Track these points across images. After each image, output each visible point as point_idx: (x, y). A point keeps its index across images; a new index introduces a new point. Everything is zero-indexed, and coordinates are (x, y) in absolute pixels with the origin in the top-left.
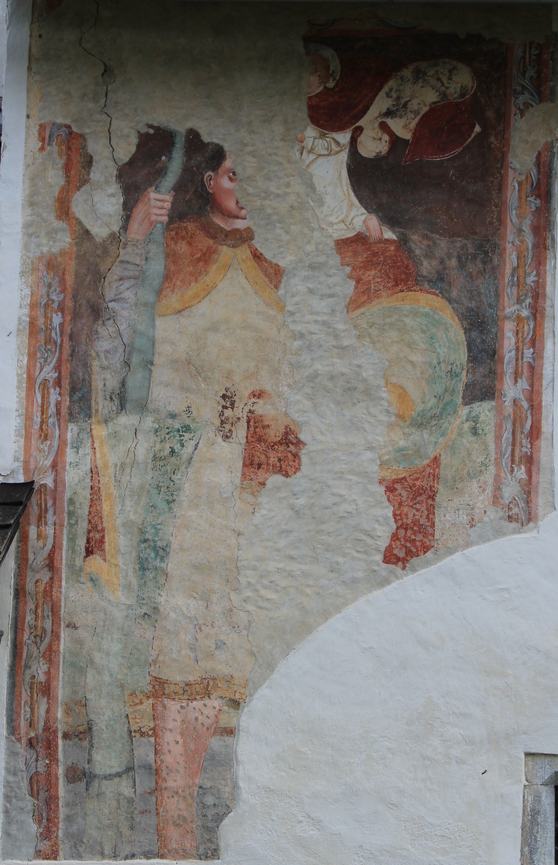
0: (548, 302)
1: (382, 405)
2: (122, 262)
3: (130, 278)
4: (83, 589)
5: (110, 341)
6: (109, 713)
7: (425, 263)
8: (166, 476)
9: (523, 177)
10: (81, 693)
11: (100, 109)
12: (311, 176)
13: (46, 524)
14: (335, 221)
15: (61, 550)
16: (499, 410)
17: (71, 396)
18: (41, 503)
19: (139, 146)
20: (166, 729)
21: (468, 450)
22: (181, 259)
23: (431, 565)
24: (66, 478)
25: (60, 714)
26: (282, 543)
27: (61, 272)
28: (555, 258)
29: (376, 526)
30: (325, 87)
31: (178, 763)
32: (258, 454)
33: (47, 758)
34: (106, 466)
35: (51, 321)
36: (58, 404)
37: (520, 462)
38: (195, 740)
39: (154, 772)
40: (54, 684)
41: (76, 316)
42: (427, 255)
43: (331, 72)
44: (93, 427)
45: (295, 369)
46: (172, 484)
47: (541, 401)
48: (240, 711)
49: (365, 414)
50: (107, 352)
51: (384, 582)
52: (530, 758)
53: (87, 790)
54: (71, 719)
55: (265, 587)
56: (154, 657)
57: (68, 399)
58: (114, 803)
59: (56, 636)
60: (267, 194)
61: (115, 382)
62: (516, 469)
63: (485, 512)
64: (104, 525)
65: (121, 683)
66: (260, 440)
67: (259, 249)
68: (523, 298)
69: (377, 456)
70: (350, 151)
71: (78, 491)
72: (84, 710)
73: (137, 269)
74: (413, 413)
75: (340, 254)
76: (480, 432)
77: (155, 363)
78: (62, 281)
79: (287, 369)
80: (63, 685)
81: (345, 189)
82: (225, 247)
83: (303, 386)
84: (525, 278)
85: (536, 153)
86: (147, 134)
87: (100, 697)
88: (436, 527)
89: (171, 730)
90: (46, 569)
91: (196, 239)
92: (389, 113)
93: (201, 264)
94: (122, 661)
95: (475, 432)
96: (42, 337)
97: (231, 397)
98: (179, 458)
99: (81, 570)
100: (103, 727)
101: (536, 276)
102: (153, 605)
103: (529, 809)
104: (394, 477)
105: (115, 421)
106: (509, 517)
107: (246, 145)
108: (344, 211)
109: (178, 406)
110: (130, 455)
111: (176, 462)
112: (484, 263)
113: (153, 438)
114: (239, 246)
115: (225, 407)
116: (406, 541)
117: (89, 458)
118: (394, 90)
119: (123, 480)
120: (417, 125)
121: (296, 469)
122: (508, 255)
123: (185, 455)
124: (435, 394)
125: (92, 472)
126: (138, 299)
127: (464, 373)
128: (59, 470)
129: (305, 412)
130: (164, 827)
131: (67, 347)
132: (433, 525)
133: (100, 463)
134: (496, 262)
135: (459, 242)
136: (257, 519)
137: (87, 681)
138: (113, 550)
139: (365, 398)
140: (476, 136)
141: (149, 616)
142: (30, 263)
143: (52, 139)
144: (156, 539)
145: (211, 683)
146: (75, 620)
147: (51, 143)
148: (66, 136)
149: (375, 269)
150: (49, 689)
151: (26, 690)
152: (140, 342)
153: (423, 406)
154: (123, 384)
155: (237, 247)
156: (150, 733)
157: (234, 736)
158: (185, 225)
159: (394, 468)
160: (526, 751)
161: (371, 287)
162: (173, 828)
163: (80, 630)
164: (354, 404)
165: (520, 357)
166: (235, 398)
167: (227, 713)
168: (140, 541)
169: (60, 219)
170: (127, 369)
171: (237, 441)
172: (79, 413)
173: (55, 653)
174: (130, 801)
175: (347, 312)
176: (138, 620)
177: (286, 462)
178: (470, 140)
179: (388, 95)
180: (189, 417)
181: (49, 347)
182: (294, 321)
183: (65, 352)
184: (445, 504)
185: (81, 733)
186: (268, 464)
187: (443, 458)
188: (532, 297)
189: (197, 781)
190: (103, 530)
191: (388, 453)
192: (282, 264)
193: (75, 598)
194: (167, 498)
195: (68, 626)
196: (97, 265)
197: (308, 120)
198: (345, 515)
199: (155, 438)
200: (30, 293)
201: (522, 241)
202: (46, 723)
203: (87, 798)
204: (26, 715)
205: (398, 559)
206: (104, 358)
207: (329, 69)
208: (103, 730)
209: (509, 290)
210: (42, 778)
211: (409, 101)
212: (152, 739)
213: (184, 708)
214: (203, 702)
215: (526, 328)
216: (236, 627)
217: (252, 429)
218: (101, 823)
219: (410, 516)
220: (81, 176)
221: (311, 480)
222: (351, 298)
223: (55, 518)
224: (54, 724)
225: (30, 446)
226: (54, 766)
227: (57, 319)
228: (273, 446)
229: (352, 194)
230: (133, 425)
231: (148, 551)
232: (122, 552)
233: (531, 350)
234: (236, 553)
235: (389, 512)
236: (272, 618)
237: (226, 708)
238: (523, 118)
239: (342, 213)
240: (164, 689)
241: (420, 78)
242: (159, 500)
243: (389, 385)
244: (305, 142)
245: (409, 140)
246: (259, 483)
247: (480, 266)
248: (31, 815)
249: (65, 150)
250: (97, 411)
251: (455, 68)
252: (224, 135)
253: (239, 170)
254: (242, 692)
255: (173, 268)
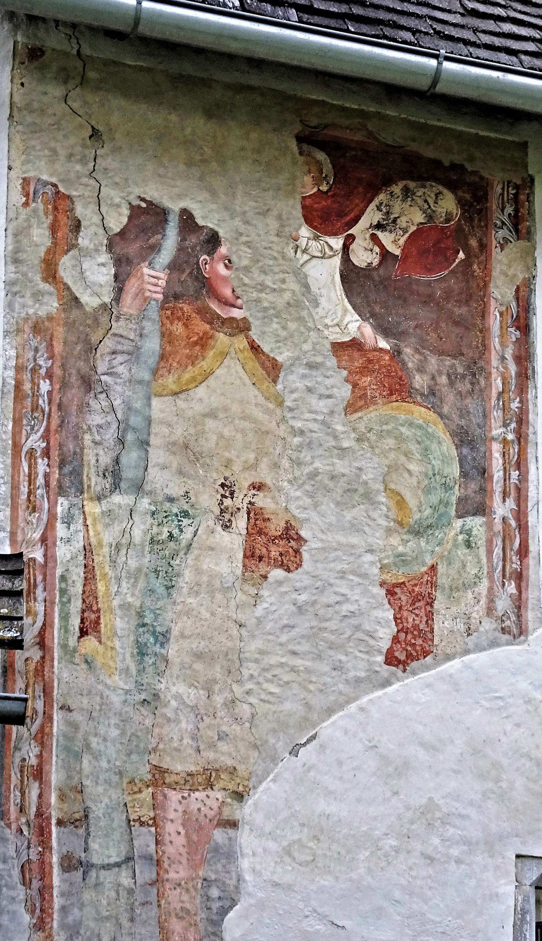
0: (531, 430)
1: (381, 510)
2: (115, 335)
3: (123, 353)
4: (76, 670)
5: (102, 416)
6: (106, 800)
7: (417, 377)
8: (164, 561)
9: (504, 309)
10: (76, 778)
11: (88, 173)
12: (306, 276)
13: (35, 600)
14: (330, 323)
15: (53, 628)
16: (489, 526)
17: (60, 468)
18: (29, 578)
19: (130, 218)
20: (167, 819)
21: (463, 562)
22: (177, 340)
23: (431, 670)
24: (58, 554)
25: (53, 799)
26: (284, 638)
27: (48, 338)
28: (536, 388)
29: (378, 628)
30: (319, 189)
31: (180, 854)
32: (259, 546)
33: (39, 845)
34: (100, 544)
35: (38, 387)
36: (47, 476)
37: (510, 578)
38: (198, 831)
39: (155, 863)
40: (46, 768)
41: (65, 385)
42: (418, 369)
43: (324, 175)
44: (85, 503)
45: (295, 466)
46: (171, 569)
47: (527, 522)
48: (243, 803)
49: (365, 517)
50: (100, 426)
51: (387, 683)
52: (519, 860)
53: (84, 879)
54: (66, 805)
55: (267, 681)
56: (154, 745)
57: (57, 472)
58: (113, 894)
59: (48, 718)
60: (262, 288)
61: (109, 459)
62: (507, 584)
63: (480, 622)
64: (99, 606)
65: (120, 770)
66: (260, 532)
67: (256, 341)
68: (508, 422)
69: (377, 558)
70: (342, 257)
71: (71, 569)
72: (79, 796)
73: (131, 344)
74: (411, 520)
75: (337, 356)
76: (474, 545)
77: (151, 443)
78: (50, 347)
79: (287, 464)
80: (56, 769)
81: (339, 294)
82: (221, 334)
83: (303, 484)
84: (510, 403)
85: (515, 287)
86: (139, 207)
87: (97, 783)
88: (435, 633)
89: (172, 821)
90: (37, 647)
91: (193, 322)
92: (379, 226)
93: (197, 348)
94: (120, 748)
95: (468, 545)
96: (28, 402)
97: (231, 487)
98: (178, 543)
99: (75, 650)
100: (101, 815)
101: (519, 402)
102: (153, 692)
103: (519, 909)
104: (394, 581)
105: (108, 499)
106: (503, 629)
107: (241, 234)
108: (339, 316)
109: (176, 491)
110: (125, 536)
111: (175, 547)
112: (472, 384)
113: (150, 520)
114: (236, 335)
115: (223, 496)
116: (407, 644)
117: (81, 534)
118: (384, 204)
119: (119, 561)
120: (406, 242)
121: (298, 565)
122: (493, 380)
123: (184, 541)
124: (431, 504)
125: (85, 549)
126: (132, 376)
127: (457, 487)
128: (49, 545)
129: (305, 509)
130: (166, 919)
131: (56, 417)
132: (432, 631)
133: (93, 541)
134: (483, 382)
135: (448, 362)
136: (259, 611)
137: (83, 766)
138: (109, 632)
139: (365, 501)
140: (460, 262)
141: (148, 702)
142: (14, 323)
143: (36, 195)
144: (155, 624)
145: (214, 775)
146: (70, 702)
147: (36, 199)
148: (52, 194)
149: (371, 376)
150: (41, 773)
151: (15, 774)
152: (135, 421)
153: (419, 514)
154: (117, 461)
155: (233, 336)
156: (151, 822)
157: (238, 829)
158: (181, 305)
159: (394, 572)
160: (518, 853)
161: (367, 393)
162: (175, 920)
163: (74, 713)
164: (354, 506)
165: (507, 477)
166: (235, 488)
167: (230, 805)
168: (138, 625)
169: (47, 282)
170: (121, 446)
171: (237, 532)
172: (69, 488)
173: (48, 735)
174: (131, 892)
175: (345, 414)
176: (136, 706)
177: (288, 557)
178: (454, 265)
179: (379, 208)
180: (187, 502)
181: (36, 415)
182: (294, 418)
183: (54, 422)
184: (443, 612)
185: (77, 820)
186: (270, 558)
187: (439, 567)
188: (517, 422)
189: (201, 873)
190: (98, 610)
191: (387, 557)
192: (279, 359)
193: (69, 680)
194: (166, 583)
195: (61, 708)
196: (87, 335)
197: (303, 220)
198: (348, 614)
199: (152, 521)
200: (15, 354)
201: (506, 368)
202: (38, 810)
203: (84, 888)
204: (16, 800)
205: (399, 662)
206: (96, 433)
207: (322, 173)
208: (100, 818)
209: (495, 413)
210: (35, 867)
211: (399, 217)
212: (153, 829)
213: (186, 799)
214: (206, 793)
215: (511, 451)
216: (239, 719)
217: (252, 521)
218: (99, 915)
219: (411, 620)
220: (69, 240)
221: (314, 577)
222: (348, 401)
223: (45, 594)
224: (47, 809)
225: (17, 517)
226: (48, 854)
227: (45, 386)
228: (274, 540)
229: (346, 300)
230: (129, 505)
231: (147, 636)
232: (119, 635)
233: (517, 472)
234: (238, 644)
235: (390, 615)
236: (275, 712)
237: (229, 800)
238: (503, 252)
239: (337, 317)
240: (164, 778)
241: (409, 197)
242: (158, 585)
243: (388, 491)
244: (299, 241)
245: (398, 256)
246: (261, 575)
247: (469, 386)
248: (24, 905)
249: (51, 210)
250: (89, 487)
251: (440, 193)
252: (219, 220)
253: (234, 259)
254: (245, 784)
255: (168, 348)
